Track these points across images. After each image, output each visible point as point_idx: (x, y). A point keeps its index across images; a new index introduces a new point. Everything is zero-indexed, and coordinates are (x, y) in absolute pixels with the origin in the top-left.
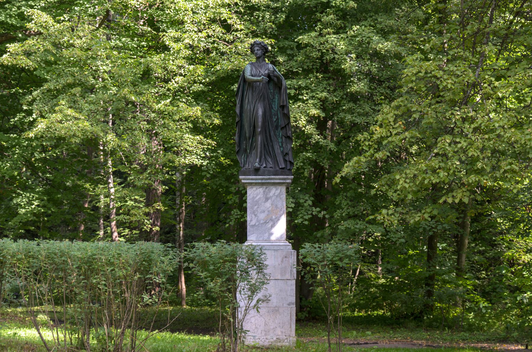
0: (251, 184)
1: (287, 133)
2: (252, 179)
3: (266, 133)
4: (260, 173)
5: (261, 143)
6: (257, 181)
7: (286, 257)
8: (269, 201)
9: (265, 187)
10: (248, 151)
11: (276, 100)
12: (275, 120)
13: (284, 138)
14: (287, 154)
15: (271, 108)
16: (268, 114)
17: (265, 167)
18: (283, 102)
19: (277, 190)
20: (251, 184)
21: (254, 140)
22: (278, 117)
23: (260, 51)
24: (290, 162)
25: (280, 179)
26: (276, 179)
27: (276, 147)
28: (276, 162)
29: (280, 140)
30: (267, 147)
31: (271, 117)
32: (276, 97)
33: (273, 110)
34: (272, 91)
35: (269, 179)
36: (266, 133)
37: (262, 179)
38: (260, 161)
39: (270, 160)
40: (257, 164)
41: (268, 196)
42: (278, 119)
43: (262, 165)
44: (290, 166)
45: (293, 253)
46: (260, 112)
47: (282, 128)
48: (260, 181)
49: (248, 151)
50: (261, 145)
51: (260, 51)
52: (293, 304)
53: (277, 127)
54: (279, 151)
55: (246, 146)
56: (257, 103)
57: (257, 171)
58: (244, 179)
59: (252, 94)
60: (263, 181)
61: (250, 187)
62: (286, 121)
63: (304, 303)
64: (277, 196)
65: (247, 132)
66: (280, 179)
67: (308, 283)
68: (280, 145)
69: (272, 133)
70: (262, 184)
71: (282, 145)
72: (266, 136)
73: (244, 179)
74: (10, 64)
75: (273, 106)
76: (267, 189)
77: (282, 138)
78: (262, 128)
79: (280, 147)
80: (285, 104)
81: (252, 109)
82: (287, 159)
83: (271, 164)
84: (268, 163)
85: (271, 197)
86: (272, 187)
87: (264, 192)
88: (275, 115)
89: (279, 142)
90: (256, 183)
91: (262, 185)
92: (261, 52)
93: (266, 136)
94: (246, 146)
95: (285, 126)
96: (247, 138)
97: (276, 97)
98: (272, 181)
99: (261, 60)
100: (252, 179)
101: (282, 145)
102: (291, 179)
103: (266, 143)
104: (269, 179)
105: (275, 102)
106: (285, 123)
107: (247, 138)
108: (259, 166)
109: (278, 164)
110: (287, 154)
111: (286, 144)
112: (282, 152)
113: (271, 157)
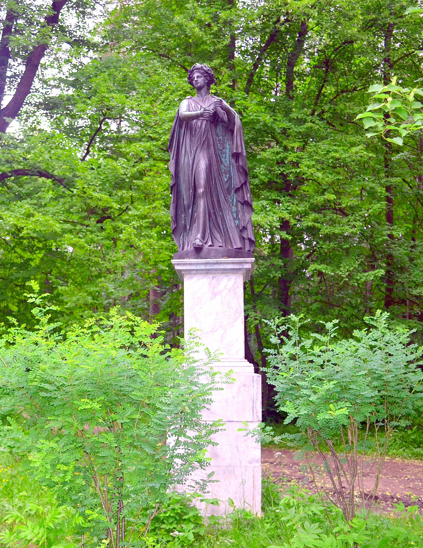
0: (189, 271)
1: (244, 197)
2: (190, 264)
3: (212, 197)
4: (202, 254)
5: (205, 210)
6: (198, 267)
7: (244, 385)
8: (218, 297)
9: (211, 276)
10: (188, 227)
11: (227, 151)
12: (226, 180)
13: (239, 205)
14: (245, 228)
15: (219, 162)
16: (215, 168)
17: (210, 246)
18: (237, 148)
19: (229, 280)
20: (189, 271)
21: (195, 209)
22: (230, 174)
23: (202, 79)
24: (250, 240)
25: (233, 263)
26: (228, 263)
27: (229, 218)
28: (227, 239)
29: (234, 209)
30: (214, 217)
31: (220, 175)
32: (228, 147)
33: (222, 166)
34: (221, 138)
35: (217, 263)
36: (212, 197)
37: (206, 264)
38: (203, 237)
39: (218, 236)
40: (198, 240)
41: (216, 290)
42: (230, 178)
43: (206, 243)
44: (250, 246)
45: (255, 379)
46: (203, 164)
47: (237, 190)
48: (203, 267)
49: (188, 227)
50: (205, 214)
51: (202, 79)
52: (257, 462)
53: (229, 191)
54: (233, 224)
55: (185, 221)
56: (198, 152)
57: (198, 250)
58: (178, 264)
59: (191, 140)
60: (208, 267)
61: (189, 276)
62: (242, 180)
63: (234, 255)
64: (230, 290)
65: (185, 197)
66: (233, 263)
67: (272, 431)
68: (235, 216)
69: (222, 198)
70: (207, 272)
71: (237, 215)
72: (212, 202)
73: (178, 264)
74: (203, 380)
75: (223, 160)
76: (215, 279)
77: (237, 206)
78: (205, 188)
79: (235, 219)
80: (240, 151)
81: (191, 162)
82: (245, 236)
83: (219, 242)
84: (215, 241)
85: (220, 292)
86: (221, 276)
87: (210, 283)
88: (226, 173)
89: (232, 213)
90: (197, 270)
91: (207, 273)
92: (204, 80)
93: (212, 202)
94: (185, 221)
95: (242, 186)
96: (186, 207)
97: (228, 147)
98: (222, 267)
99: (203, 91)
100: (190, 264)
101: (237, 215)
102: (251, 263)
103: (212, 211)
104: (217, 263)
105: (225, 153)
106: (240, 182)
107: (186, 207)
108: (200, 244)
109: (231, 243)
110: (245, 228)
111: (243, 213)
112: (237, 227)
113: (220, 232)
